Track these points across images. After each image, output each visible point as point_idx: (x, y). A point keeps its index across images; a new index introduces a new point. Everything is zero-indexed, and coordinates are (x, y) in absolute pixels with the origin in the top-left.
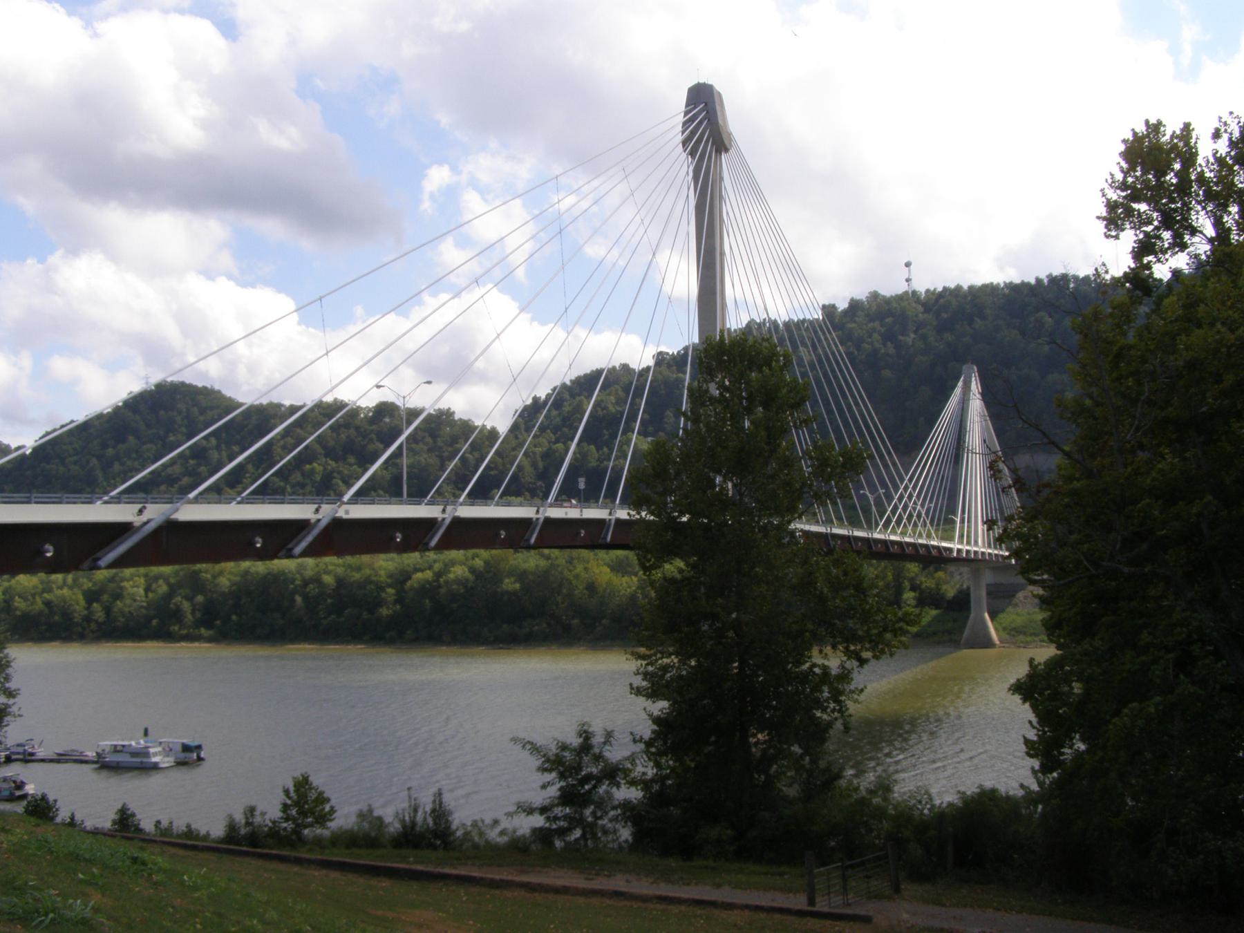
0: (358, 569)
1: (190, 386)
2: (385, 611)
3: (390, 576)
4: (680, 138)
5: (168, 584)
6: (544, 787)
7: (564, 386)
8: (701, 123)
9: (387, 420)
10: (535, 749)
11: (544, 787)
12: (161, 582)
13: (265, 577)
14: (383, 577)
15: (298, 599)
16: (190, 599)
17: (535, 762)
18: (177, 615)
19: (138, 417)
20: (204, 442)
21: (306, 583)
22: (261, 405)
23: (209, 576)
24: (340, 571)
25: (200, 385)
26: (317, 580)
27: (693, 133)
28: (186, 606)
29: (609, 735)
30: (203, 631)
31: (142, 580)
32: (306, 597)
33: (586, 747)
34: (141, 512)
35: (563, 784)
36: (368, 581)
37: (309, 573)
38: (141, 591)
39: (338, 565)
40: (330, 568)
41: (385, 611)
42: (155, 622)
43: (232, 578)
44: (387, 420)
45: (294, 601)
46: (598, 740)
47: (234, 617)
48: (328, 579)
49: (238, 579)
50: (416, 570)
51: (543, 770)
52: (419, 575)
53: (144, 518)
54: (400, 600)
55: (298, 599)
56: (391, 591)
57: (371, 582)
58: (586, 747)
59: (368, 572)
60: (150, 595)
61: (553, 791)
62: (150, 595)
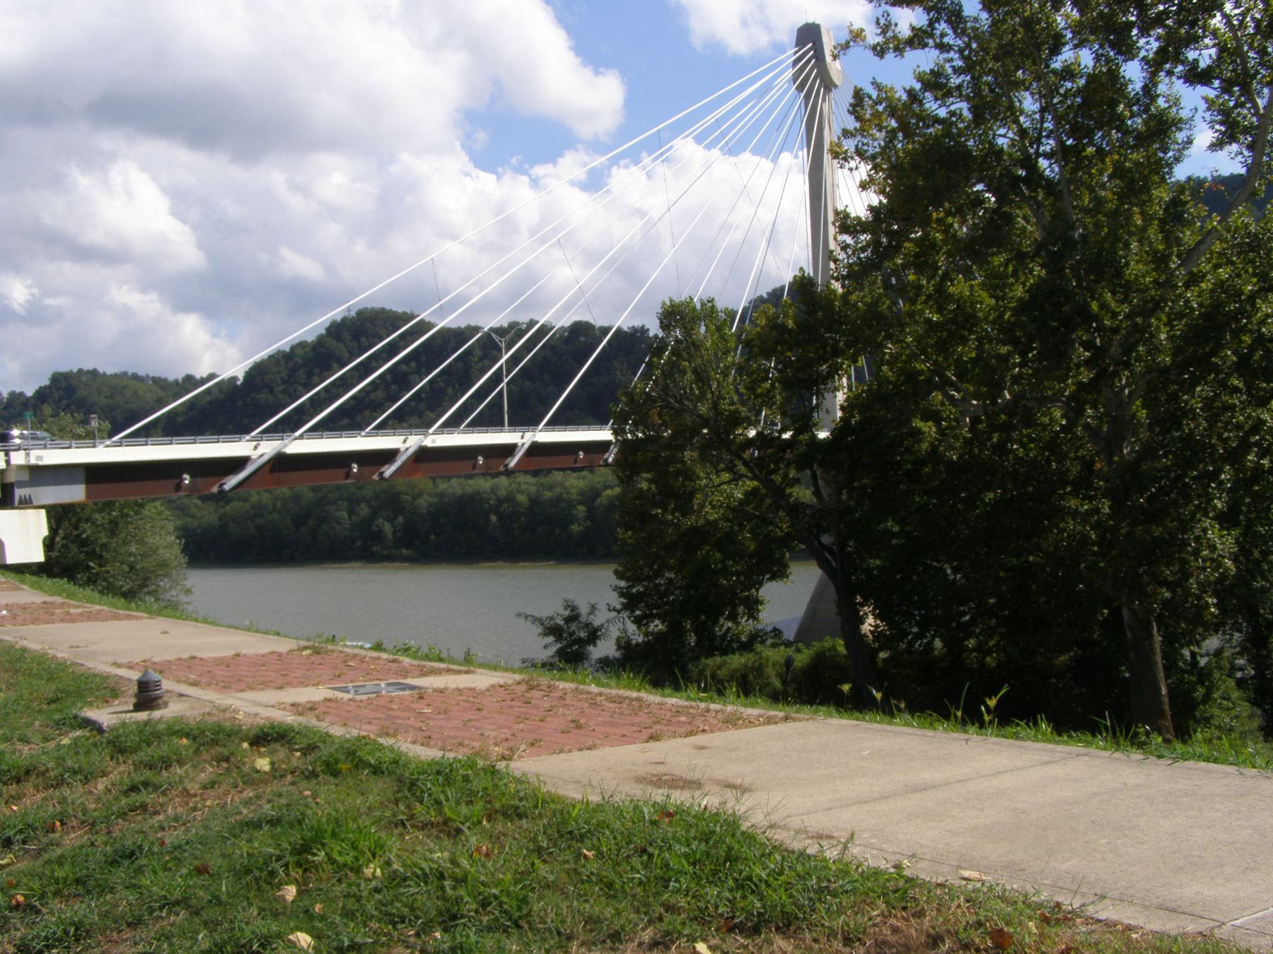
0: (551, 488)
1: (390, 311)
2: (575, 528)
3: (581, 493)
4: (790, 73)
5: (371, 507)
6: (546, 647)
7: (125, 373)
8: (809, 61)
9: (582, 339)
10: (536, 620)
11: (546, 647)
12: (363, 505)
13: (461, 497)
14: (574, 494)
15: (494, 518)
16: (391, 520)
17: (540, 630)
18: (379, 536)
19: (340, 345)
20: (460, 365)
21: (500, 502)
22: (459, 328)
23: (409, 498)
24: (533, 489)
25: (400, 311)
26: (510, 499)
27: (801, 70)
28: (388, 528)
29: (593, 609)
30: (404, 551)
31: (346, 504)
32: (500, 516)
33: (573, 617)
34: (405, 441)
35: (559, 646)
36: (559, 499)
37: (503, 493)
38: (345, 514)
39: (532, 484)
40: (523, 487)
41: (575, 528)
42: (358, 544)
43: (430, 499)
44: (582, 339)
45: (488, 520)
46: (584, 610)
47: (432, 537)
48: (521, 498)
49: (436, 500)
50: (606, 487)
51: (546, 635)
52: (609, 492)
53: (407, 445)
54: (590, 516)
55: (494, 518)
56: (581, 508)
57: (562, 500)
58: (573, 617)
59: (558, 490)
60: (354, 518)
61: (552, 650)
62: (354, 518)
